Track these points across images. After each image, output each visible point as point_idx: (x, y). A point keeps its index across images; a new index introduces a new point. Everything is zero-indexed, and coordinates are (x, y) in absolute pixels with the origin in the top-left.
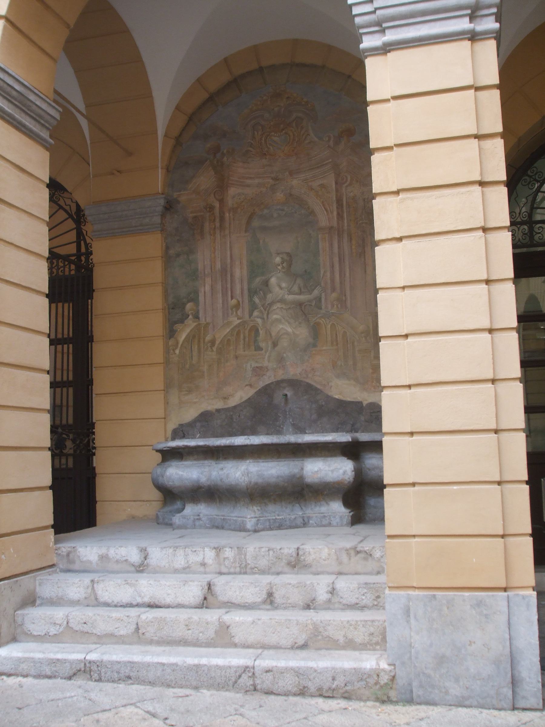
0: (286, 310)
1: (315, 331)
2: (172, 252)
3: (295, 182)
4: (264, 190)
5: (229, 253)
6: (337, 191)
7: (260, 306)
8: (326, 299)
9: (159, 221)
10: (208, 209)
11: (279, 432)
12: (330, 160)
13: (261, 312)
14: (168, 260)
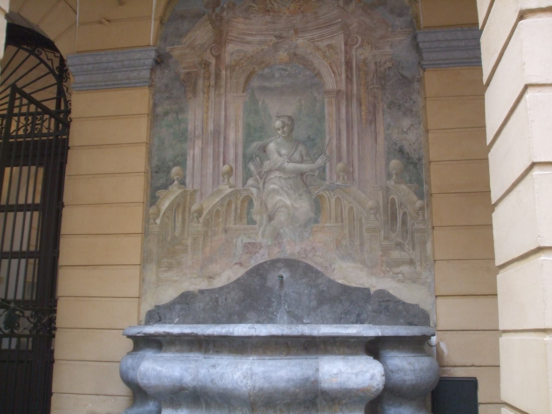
0: (285, 179)
1: (318, 205)
2: (159, 110)
3: (300, 41)
4: (265, 47)
5: (223, 113)
6: (346, 52)
7: (255, 174)
8: (331, 170)
9: (148, 75)
10: (203, 65)
11: (271, 320)
12: (340, 20)
13: (257, 180)
14: (154, 118)
